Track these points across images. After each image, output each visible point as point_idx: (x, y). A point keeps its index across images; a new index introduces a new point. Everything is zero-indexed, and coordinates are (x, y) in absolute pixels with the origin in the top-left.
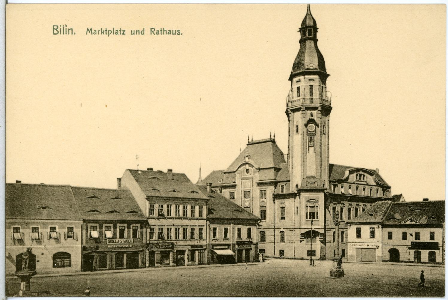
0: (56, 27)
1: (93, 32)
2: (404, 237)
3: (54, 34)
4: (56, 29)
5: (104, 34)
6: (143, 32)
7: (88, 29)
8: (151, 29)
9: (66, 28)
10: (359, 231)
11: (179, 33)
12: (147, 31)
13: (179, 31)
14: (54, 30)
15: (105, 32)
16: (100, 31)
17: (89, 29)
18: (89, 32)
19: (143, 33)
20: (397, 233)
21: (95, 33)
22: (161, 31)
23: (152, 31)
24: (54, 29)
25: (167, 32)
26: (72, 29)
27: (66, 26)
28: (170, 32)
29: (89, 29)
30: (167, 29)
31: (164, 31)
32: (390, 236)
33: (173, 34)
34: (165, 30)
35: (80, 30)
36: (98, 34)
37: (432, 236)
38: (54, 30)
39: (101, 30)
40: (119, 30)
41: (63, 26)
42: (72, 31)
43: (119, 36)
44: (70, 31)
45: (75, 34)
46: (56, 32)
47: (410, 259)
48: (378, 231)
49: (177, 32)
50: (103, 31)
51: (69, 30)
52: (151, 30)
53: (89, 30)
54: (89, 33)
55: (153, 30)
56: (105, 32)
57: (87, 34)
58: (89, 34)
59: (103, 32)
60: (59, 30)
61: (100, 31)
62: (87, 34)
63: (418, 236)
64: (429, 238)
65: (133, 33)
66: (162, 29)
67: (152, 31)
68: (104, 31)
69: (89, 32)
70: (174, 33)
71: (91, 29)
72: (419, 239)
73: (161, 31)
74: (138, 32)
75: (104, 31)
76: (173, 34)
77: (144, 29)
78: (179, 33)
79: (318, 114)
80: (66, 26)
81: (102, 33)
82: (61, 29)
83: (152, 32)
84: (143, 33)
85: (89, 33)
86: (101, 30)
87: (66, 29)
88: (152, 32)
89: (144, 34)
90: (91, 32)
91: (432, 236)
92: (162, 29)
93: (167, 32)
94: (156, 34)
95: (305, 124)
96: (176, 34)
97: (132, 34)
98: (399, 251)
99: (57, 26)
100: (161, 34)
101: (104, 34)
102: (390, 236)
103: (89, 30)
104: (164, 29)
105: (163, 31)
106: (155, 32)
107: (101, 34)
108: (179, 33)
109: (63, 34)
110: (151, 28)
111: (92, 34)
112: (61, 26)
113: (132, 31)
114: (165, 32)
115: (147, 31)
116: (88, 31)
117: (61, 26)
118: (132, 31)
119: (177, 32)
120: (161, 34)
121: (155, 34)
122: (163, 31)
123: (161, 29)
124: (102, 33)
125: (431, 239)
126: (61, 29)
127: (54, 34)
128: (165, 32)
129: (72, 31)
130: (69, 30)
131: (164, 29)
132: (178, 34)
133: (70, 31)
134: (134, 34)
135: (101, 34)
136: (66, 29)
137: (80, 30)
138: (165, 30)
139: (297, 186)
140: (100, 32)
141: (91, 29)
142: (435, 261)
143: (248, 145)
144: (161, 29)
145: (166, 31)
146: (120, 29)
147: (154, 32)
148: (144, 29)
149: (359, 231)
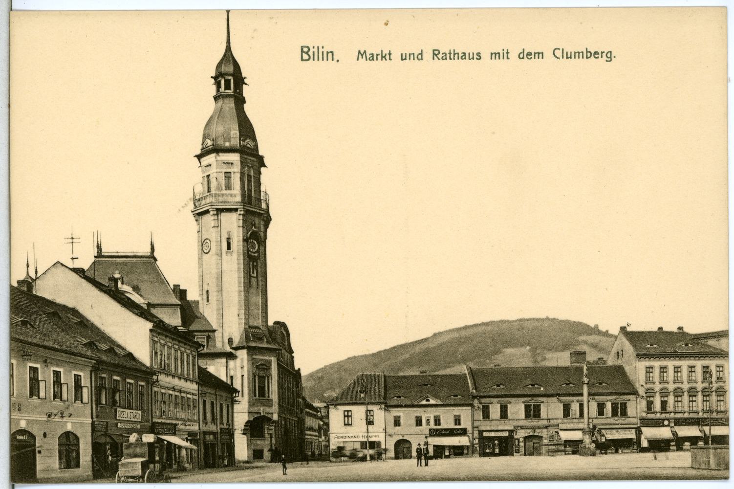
0: (306, 50)
1: (368, 56)
2: (419, 422)
3: (302, 60)
4: (307, 53)
5: (386, 60)
6: (420, 56)
7: (359, 52)
8: (434, 50)
9: (323, 50)
10: (348, 415)
11: (479, 58)
12: (427, 56)
13: (480, 53)
14: (303, 53)
15: (387, 57)
16: (379, 55)
17: (362, 52)
18: (362, 55)
19: (420, 57)
20: (407, 415)
21: (372, 57)
22: (450, 53)
23: (435, 54)
24: (302, 51)
25: (461, 55)
26: (332, 52)
27: (323, 47)
28: (373, 56)
29: (362, 52)
30: (460, 51)
31: (455, 54)
32: (397, 422)
33: (470, 59)
34: (456, 52)
35: (346, 53)
36: (377, 60)
37: (457, 420)
38: (303, 53)
39: (382, 53)
40: (448, 52)
41: (318, 47)
42: (333, 55)
43: (379, 62)
44: (330, 55)
45: (338, 61)
46: (305, 57)
47: (493, 405)
48: (379, 414)
49: (475, 56)
50: (384, 55)
51: (328, 53)
52: (302, 50)
53: (361, 54)
54: (362, 57)
55: (436, 52)
56: (387, 57)
57: (358, 60)
58: (362, 60)
59: (383, 57)
60: (311, 53)
61: (379, 55)
62: (358, 60)
63: (437, 421)
64: (453, 422)
65: (404, 57)
66: (452, 52)
67: (435, 54)
68: (386, 55)
69: (362, 55)
70: (569, 56)
71: (365, 52)
72: (439, 424)
73: (450, 53)
74: (412, 56)
75: (386, 55)
76: (567, 58)
77: (422, 50)
78: (479, 58)
79: (218, 259)
80: (323, 47)
81: (384, 59)
82: (314, 52)
83: (435, 56)
84: (420, 57)
85: (362, 57)
86: (382, 53)
87: (323, 52)
88: (435, 56)
89: (422, 59)
90: (364, 56)
91: (457, 420)
92: (452, 52)
93: (461, 55)
94: (441, 59)
95: (179, 286)
96: (600, 53)
97: (402, 60)
98: (395, 442)
99: (308, 47)
100: (450, 59)
101: (386, 60)
102: (397, 422)
103: (361, 54)
104: (454, 51)
105: (452, 55)
106: (440, 56)
107: (382, 60)
108: (610, 56)
109: (318, 60)
110: (612, 52)
111: (366, 60)
112: (314, 47)
113: (402, 55)
114: (456, 56)
115: (427, 56)
116: (360, 56)
117: (314, 47)
118: (402, 55)
119: (475, 56)
120: (450, 59)
121: (439, 59)
122: (452, 55)
123: (450, 51)
124: (384, 59)
125: (456, 424)
126: (314, 52)
127: (302, 60)
128: (456, 56)
129: (333, 55)
130: (328, 53)
131: (454, 51)
132: (477, 59)
133: (330, 55)
134: (571, 57)
135: (382, 60)
136: (323, 52)
137: (346, 53)
138: (456, 52)
139: (230, 341)
140: (379, 57)
141: (365, 52)
142: (525, 405)
143: (95, 257)
144: (450, 51)
145: (458, 54)
146: (390, 51)
147: (438, 56)
148: (422, 50)
149: (348, 415)
